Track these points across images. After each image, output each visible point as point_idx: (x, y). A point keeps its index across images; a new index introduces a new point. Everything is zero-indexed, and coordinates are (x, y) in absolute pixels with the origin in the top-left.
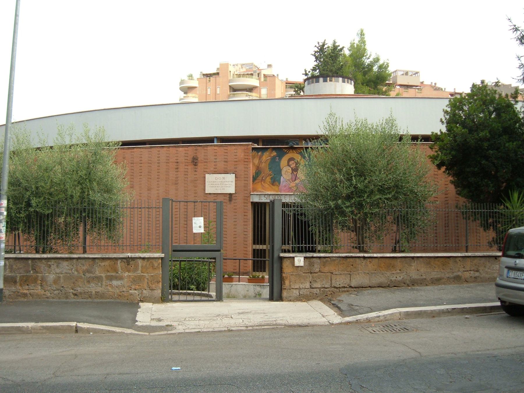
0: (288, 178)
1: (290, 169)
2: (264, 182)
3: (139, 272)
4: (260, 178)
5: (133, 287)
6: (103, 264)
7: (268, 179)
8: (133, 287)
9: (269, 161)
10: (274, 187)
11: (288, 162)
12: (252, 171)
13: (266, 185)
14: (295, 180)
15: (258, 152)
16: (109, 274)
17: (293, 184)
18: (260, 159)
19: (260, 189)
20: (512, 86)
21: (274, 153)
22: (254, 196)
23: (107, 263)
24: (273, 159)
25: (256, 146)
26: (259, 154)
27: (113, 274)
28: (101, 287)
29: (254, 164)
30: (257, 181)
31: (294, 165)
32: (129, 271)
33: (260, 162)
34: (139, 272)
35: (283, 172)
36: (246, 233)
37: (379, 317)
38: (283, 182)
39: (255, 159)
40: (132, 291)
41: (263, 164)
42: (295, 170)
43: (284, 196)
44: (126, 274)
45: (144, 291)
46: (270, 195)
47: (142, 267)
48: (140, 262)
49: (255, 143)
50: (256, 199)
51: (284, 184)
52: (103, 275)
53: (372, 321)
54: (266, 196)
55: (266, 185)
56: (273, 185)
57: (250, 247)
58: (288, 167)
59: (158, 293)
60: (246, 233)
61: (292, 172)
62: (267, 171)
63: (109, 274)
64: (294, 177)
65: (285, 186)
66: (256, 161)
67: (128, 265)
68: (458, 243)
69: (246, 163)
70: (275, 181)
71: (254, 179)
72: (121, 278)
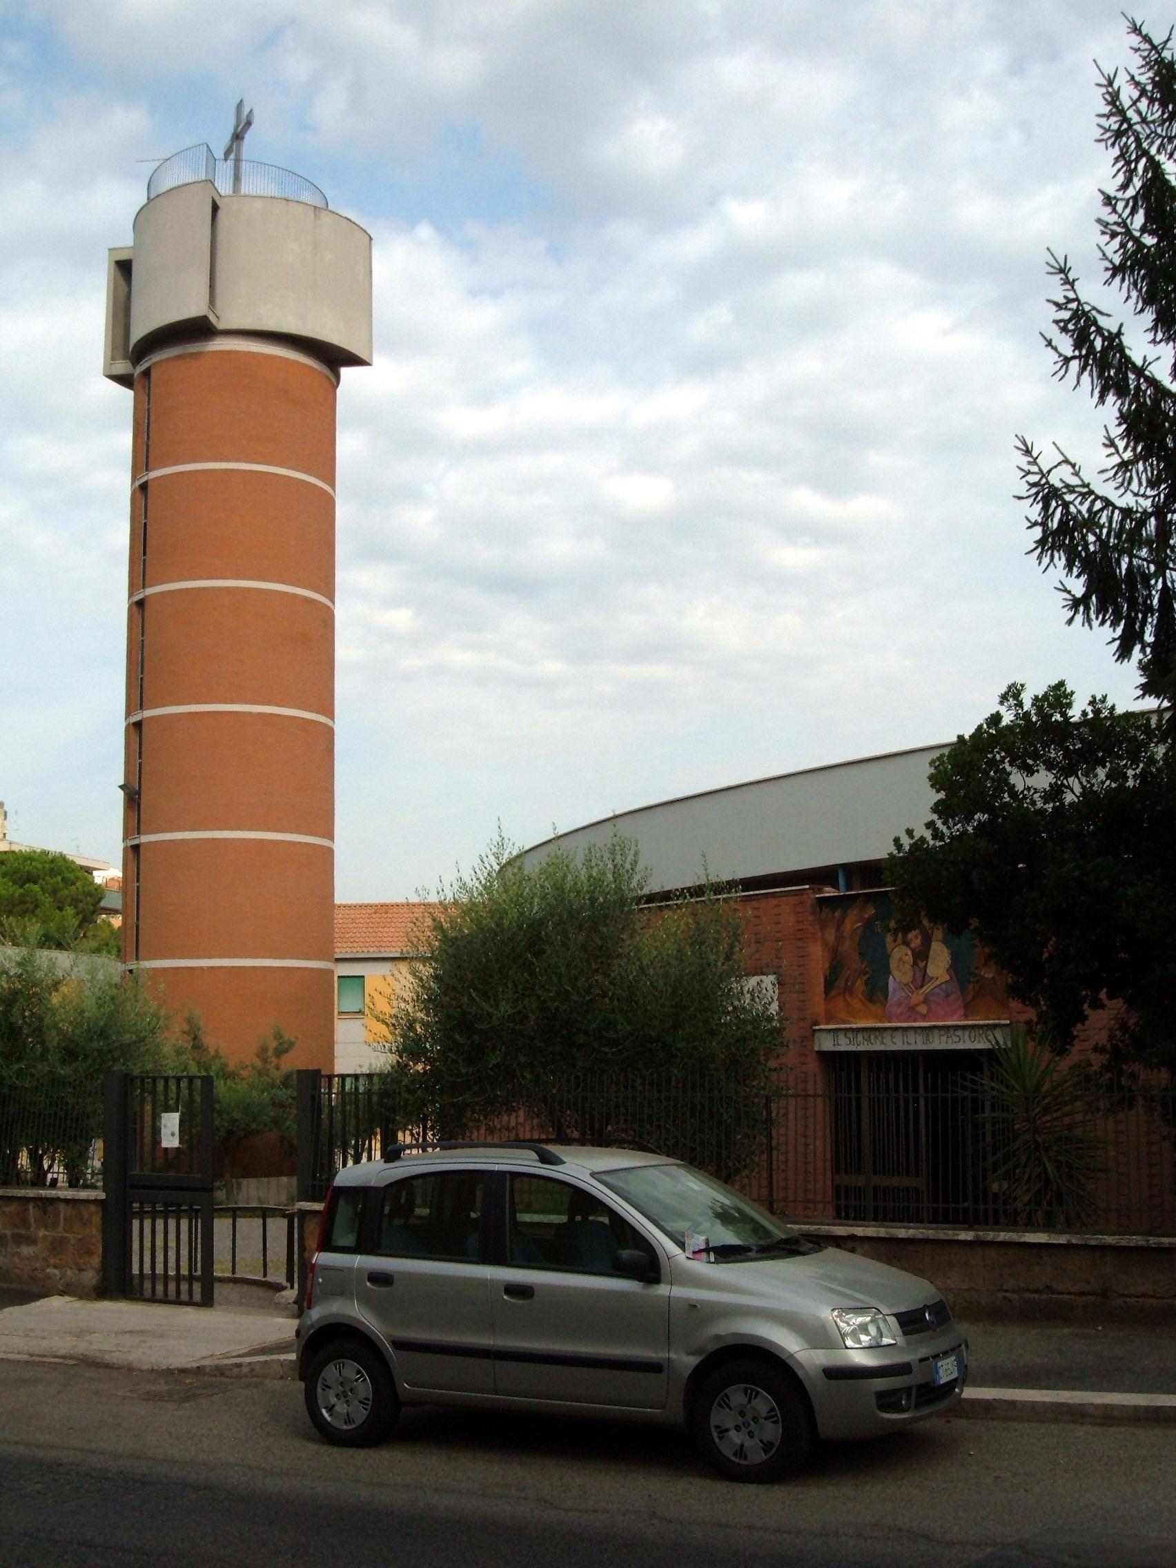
0: (904, 981)
1: (909, 952)
2: (851, 994)
3: (60, 1229)
4: (840, 983)
5: (52, 1261)
6: (7, 1209)
7: (860, 985)
8: (52, 1261)
10: (873, 1007)
12: (818, 957)
14: (922, 986)
15: (833, 910)
16: (16, 1231)
17: (916, 998)
18: (838, 928)
19: (842, 1015)
20: (1143, 680)
22: (824, 1036)
23: (12, 1208)
24: (869, 924)
25: (829, 892)
27: (23, 1232)
28: (5, 1256)
30: (834, 992)
31: (918, 941)
32: (46, 1228)
33: (840, 938)
34: (60, 1229)
35: (893, 964)
37: (239, 1365)
38: (894, 990)
40: (50, 1270)
41: (847, 943)
43: (889, 1032)
44: (42, 1233)
45: (69, 1272)
47: (65, 1219)
48: (62, 1207)
49: (827, 884)
50: (826, 1044)
52: (8, 1233)
53: (227, 1373)
55: (855, 1003)
59: (90, 1278)
61: (915, 963)
63: (16, 1231)
65: (899, 1004)
66: (831, 937)
67: (45, 1213)
68: (314, 1186)
69: (800, 944)
70: (876, 991)
71: (829, 985)
72: (31, 1241)
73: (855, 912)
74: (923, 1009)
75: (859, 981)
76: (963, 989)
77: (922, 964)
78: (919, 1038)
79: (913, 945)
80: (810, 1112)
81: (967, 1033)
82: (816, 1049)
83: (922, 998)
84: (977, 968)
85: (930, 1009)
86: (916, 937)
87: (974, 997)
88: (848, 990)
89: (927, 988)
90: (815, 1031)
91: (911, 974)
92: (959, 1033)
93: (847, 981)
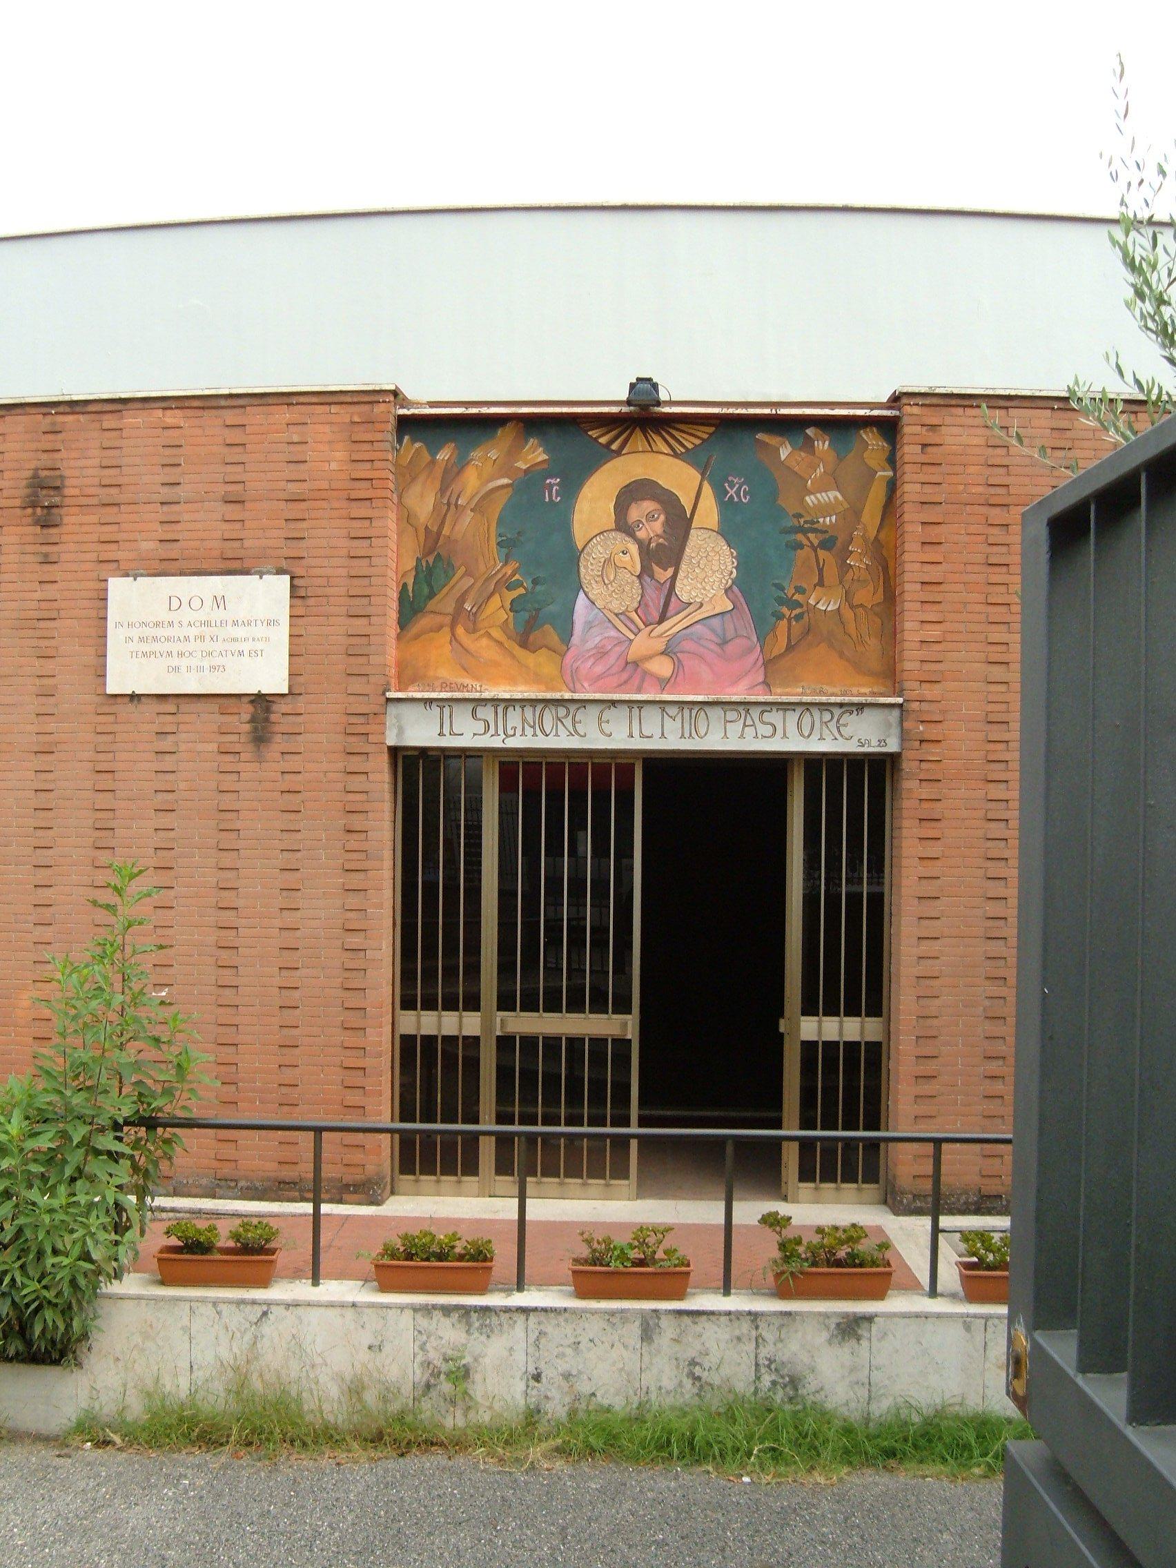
0: (616, 606)
1: (634, 548)
4: (445, 603)
7: (497, 610)
9: (502, 499)
11: (621, 507)
13: (483, 647)
17: (644, 643)
21: (535, 454)
24: (529, 483)
26: (444, 455)
29: (407, 518)
30: (424, 622)
31: (658, 526)
33: (448, 507)
36: (355, 940)
38: (589, 626)
39: (416, 489)
42: (664, 555)
46: (510, 702)
51: (595, 640)
54: (486, 713)
56: (524, 644)
57: (382, 1024)
58: (619, 536)
60: (355, 940)
61: (646, 571)
62: (492, 563)
64: (655, 601)
65: (601, 653)
66: (423, 501)
73: (493, 454)
74: (662, 667)
75: (496, 600)
76: (763, 631)
77: (664, 575)
78: (672, 727)
79: (641, 534)
80: (320, 591)
81: (792, 717)
82: (391, 741)
83: (660, 645)
84: (799, 590)
85: (678, 665)
86: (651, 517)
87: (790, 648)
88: (464, 618)
89: (673, 625)
90: (388, 700)
91: (637, 591)
92: (775, 717)
93: (461, 600)
